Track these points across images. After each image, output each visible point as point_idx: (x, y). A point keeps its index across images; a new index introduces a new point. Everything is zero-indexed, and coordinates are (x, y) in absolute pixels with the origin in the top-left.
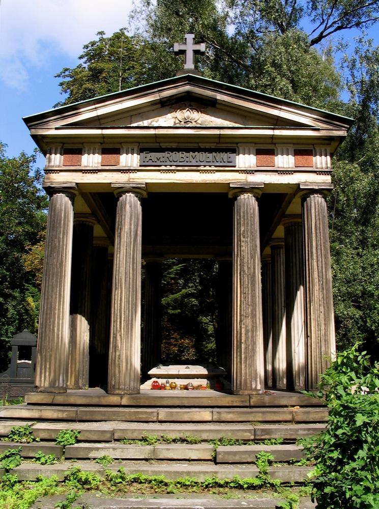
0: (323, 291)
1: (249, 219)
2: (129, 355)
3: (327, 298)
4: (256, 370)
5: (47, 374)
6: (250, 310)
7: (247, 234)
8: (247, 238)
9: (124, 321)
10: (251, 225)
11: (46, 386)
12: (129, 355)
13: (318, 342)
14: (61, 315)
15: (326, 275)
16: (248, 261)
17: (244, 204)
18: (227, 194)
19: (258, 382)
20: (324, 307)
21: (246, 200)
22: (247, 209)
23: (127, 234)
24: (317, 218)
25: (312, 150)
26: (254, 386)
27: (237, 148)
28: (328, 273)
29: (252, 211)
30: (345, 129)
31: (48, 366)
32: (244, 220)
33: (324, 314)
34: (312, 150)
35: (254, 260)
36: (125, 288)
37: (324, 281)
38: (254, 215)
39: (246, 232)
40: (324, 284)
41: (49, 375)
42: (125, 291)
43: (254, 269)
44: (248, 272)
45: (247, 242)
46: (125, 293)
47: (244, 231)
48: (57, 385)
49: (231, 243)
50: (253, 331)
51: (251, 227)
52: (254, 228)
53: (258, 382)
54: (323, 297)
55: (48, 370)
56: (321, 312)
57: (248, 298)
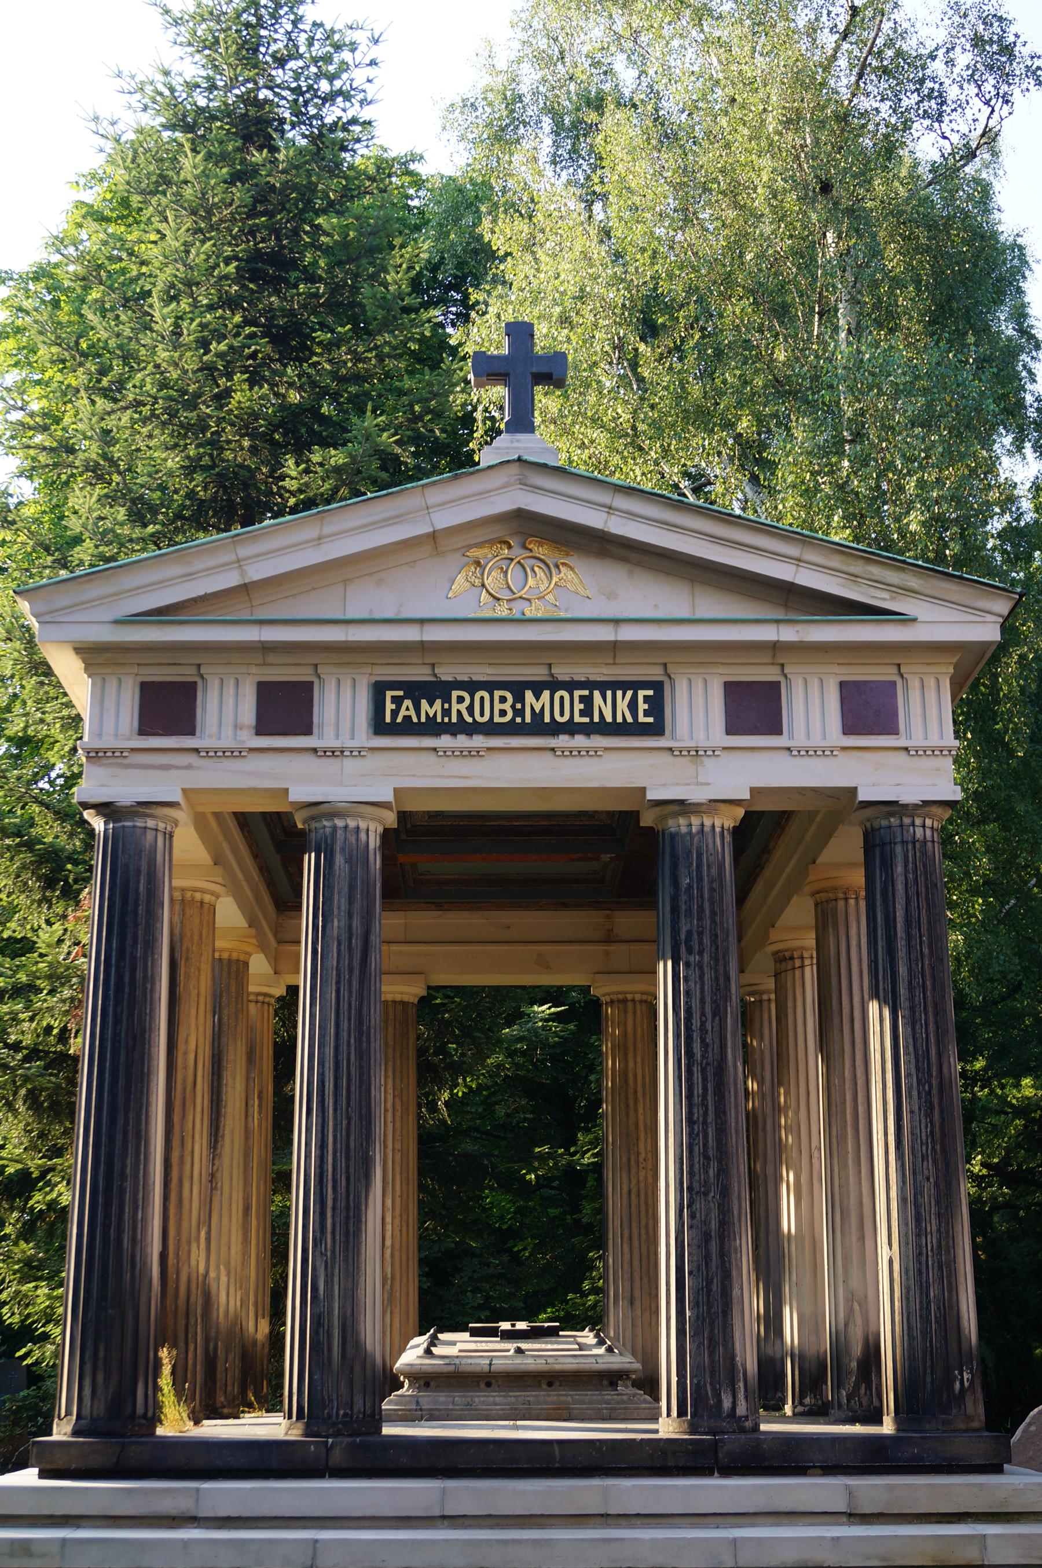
0: (929, 1115)
1: (706, 896)
2: (349, 1313)
3: (943, 1135)
4: (733, 1357)
5: (100, 1378)
6: (711, 1172)
7: (701, 943)
8: (701, 953)
9: (334, 1209)
10: (713, 913)
11: (95, 1413)
12: (349, 1313)
13: (438, 690)
14: (140, 1196)
15: (940, 1066)
16: (703, 1023)
17: (689, 853)
18: (635, 815)
19: (741, 1395)
20: (935, 1161)
21: (696, 840)
22: (699, 865)
23: (339, 945)
24: (912, 891)
25: (894, 683)
26: (727, 1404)
27: (665, 679)
28: (945, 1060)
29: (714, 871)
30: (368, 1405)
31: (102, 1354)
32: (691, 898)
33: (936, 1184)
34: (894, 683)
35: (723, 1021)
36: (335, 1110)
37: (934, 1082)
38: (721, 884)
39: (695, 936)
40: (935, 1091)
41: (106, 1380)
42: (335, 1119)
43: (723, 1047)
44: (703, 1057)
45: (701, 968)
46: (335, 1125)
47: (689, 933)
48: (128, 1410)
49: (193, 716)
50: (722, 1238)
51: (713, 921)
52: (722, 923)
53: (741, 1395)
54: (932, 1132)
55: (101, 1364)
56: (928, 1179)
57: (706, 1137)
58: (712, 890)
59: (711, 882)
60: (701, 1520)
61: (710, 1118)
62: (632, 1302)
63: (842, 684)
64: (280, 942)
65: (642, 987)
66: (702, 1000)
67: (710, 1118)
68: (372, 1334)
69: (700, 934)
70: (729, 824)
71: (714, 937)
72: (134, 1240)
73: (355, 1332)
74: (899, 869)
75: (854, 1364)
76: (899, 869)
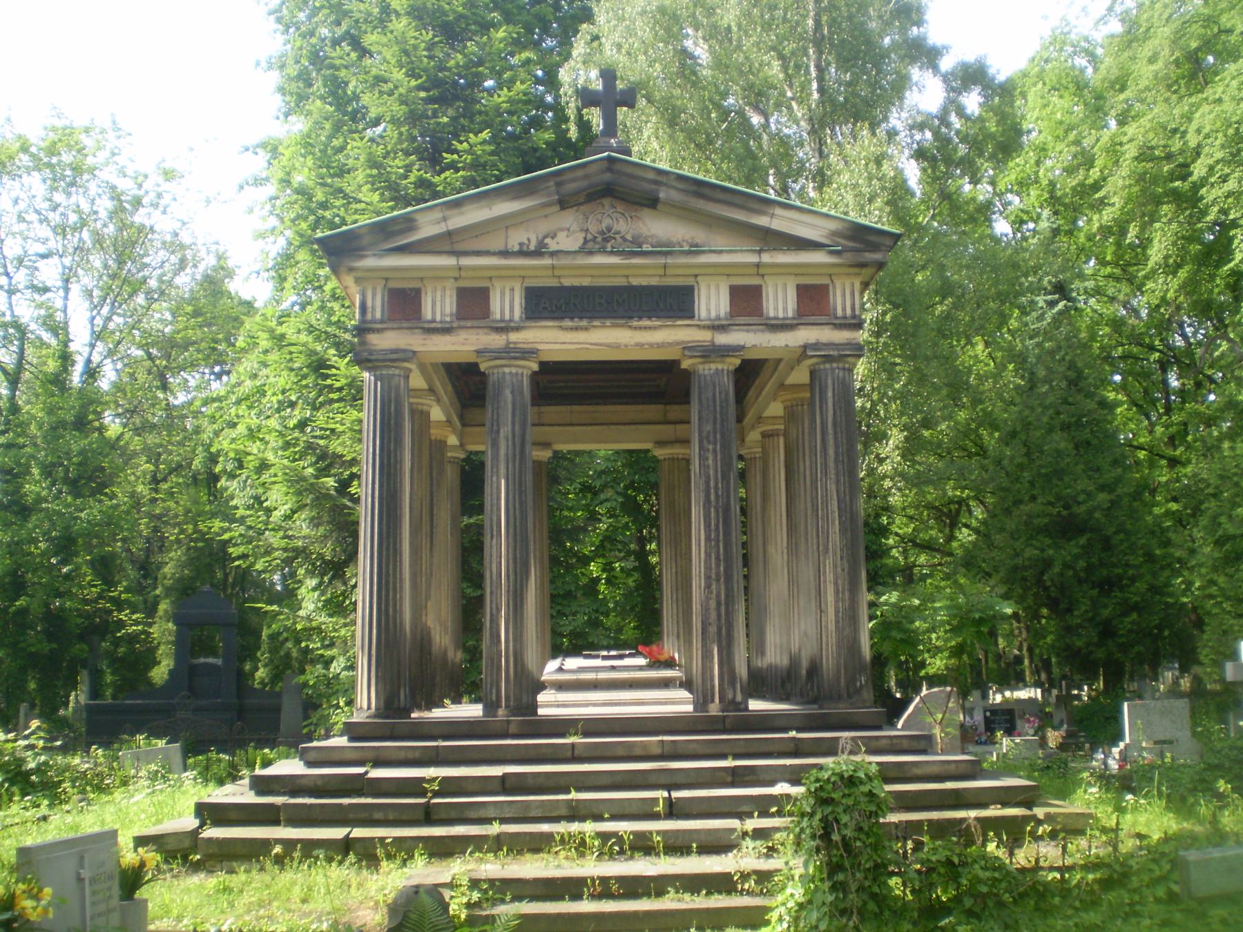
12: (425, 555)
29: (723, 396)
35: (728, 483)
58: (721, 407)
59: (721, 402)
60: (598, 753)
61: (721, 538)
62: (678, 637)
63: (798, 286)
64: (464, 425)
65: (683, 451)
66: (716, 471)
67: (721, 538)
68: (531, 656)
69: (715, 433)
70: (732, 368)
71: (723, 434)
72: (395, 611)
73: (522, 660)
74: (830, 394)
75: (804, 672)
76: (830, 394)
